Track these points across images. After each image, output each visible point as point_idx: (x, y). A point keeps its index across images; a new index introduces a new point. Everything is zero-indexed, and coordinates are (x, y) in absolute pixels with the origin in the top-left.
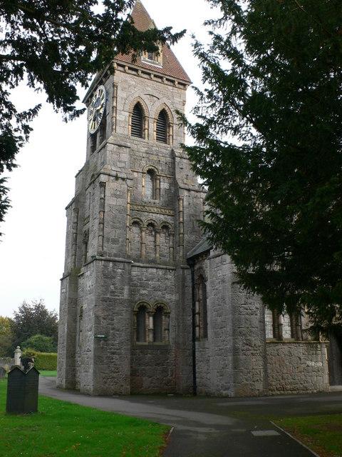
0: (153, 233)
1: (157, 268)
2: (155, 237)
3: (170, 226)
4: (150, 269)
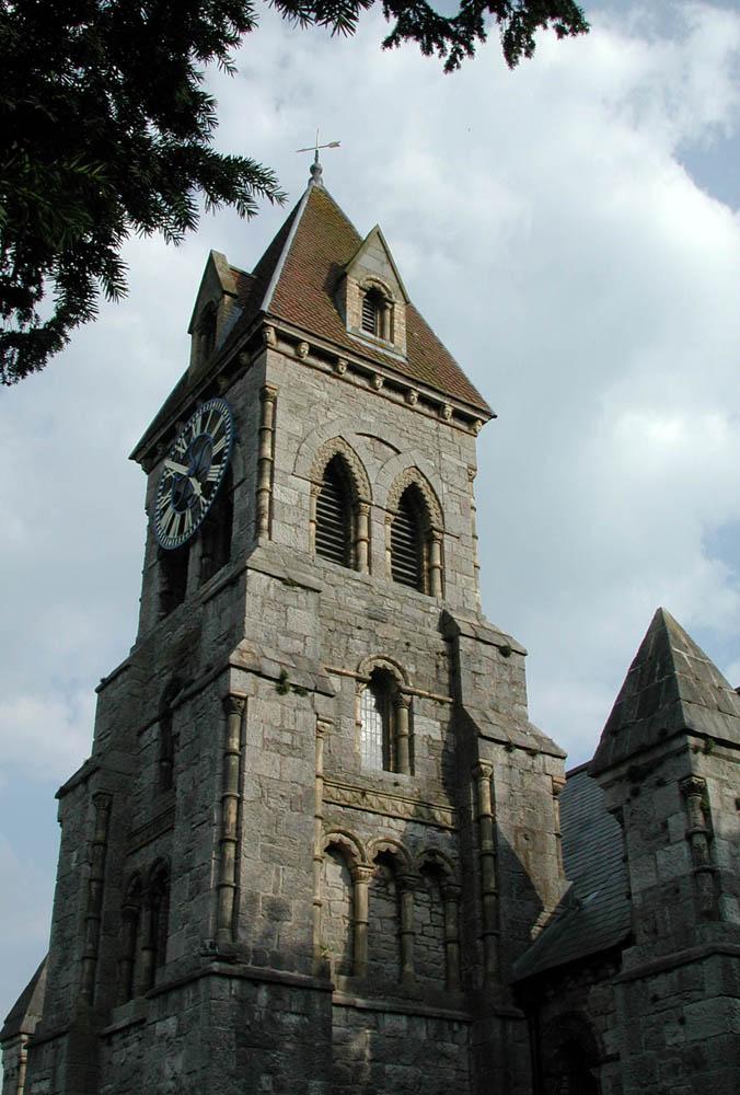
0: (392, 889)
1: (410, 1015)
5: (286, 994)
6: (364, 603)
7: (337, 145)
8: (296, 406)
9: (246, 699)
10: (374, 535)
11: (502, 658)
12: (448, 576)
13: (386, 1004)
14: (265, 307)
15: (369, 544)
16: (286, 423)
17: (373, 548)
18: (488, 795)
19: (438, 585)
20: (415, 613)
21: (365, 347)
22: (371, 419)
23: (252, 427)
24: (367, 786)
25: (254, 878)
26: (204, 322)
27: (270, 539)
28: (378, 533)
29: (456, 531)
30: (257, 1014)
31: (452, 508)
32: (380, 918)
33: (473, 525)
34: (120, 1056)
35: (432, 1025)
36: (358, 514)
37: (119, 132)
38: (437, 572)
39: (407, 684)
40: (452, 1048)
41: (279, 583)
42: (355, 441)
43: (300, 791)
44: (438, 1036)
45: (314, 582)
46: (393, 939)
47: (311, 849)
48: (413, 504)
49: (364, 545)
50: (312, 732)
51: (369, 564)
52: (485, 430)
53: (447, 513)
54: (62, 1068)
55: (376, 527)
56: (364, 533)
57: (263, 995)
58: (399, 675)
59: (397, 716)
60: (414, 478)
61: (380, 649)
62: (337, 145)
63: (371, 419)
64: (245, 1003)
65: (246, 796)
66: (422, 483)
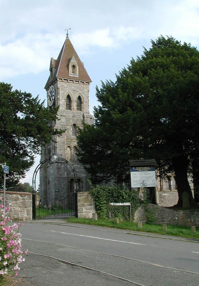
1: (77, 164)
4: (75, 165)
5: (62, 164)
6: (72, 115)
7: (70, 29)
8: (62, 89)
10: (74, 105)
11: (91, 119)
13: (75, 163)
14: (57, 76)
16: (61, 92)
19: (83, 110)
21: (71, 76)
22: (73, 87)
23: (57, 90)
24: (72, 139)
25: (58, 152)
26: (51, 70)
28: (74, 105)
31: (85, 98)
33: (88, 99)
34: (48, 169)
36: (71, 102)
37: (31, 113)
38: (83, 108)
42: (71, 92)
43: (63, 142)
45: (65, 114)
47: (65, 148)
48: (79, 98)
52: (91, 84)
53: (84, 99)
54: (43, 171)
55: (74, 104)
56: (72, 105)
57: (60, 164)
58: (76, 124)
60: (79, 95)
62: (70, 29)
63: (73, 87)
64: (58, 165)
66: (81, 95)
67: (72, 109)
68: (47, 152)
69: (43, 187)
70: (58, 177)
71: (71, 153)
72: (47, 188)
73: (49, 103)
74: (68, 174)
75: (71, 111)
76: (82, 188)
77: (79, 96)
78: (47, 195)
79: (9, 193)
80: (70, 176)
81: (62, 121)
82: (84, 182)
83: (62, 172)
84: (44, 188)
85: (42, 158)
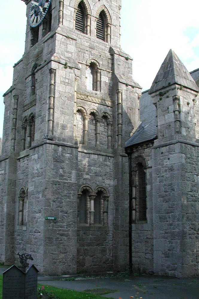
0: (94, 122)
2: (96, 125)
3: (109, 117)
4: (92, 155)
5: (66, 148)
6: (89, 44)
9: (56, 70)
11: (126, 61)
12: (112, 37)
13: (92, 152)
15: (90, 27)
17: (91, 28)
18: (121, 98)
19: (109, 40)
20: (102, 47)
24: (88, 94)
27: (62, 25)
28: (93, 24)
29: (115, 24)
30: (59, 154)
31: (114, 17)
32: (91, 130)
33: (120, 23)
34: (22, 164)
35: (104, 157)
38: (109, 36)
39: (100, 67)
40: (108, 163)
41: (65, 37)
44: (105, 160)
45: (75, 37)
46: (94, 135)
48: (103, 15)
49: (89, 27)
50: (74, 79)
51: (90, 33)
53: (112, 19)
54: (7, 167)
56: (89, 24)
57: (60, 149)
58: (97, 64)
59: (97, 75)
60: (103, 8)
61: (93, 57)
64: (55, 151)
65: (56, 96)
66: (106, 10)
67: (89, 32)
68: (20, 126)
69: (6, 205)
70: (54, 183)
71: (84, 125)
72: (15, 208)
73: (31, 22)
74: (79, 176)
75: (87, 36)
76: (105, 214)
77: (103, 10)
78: (13, 225)
79: (191, 93)
80: (81, 183)
81: (68, 50)
82: (111, 199)
83: (67, 169)
84: (8, 208)
85: (6, 140)
